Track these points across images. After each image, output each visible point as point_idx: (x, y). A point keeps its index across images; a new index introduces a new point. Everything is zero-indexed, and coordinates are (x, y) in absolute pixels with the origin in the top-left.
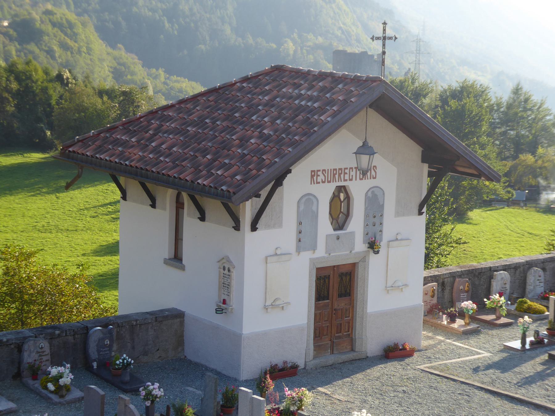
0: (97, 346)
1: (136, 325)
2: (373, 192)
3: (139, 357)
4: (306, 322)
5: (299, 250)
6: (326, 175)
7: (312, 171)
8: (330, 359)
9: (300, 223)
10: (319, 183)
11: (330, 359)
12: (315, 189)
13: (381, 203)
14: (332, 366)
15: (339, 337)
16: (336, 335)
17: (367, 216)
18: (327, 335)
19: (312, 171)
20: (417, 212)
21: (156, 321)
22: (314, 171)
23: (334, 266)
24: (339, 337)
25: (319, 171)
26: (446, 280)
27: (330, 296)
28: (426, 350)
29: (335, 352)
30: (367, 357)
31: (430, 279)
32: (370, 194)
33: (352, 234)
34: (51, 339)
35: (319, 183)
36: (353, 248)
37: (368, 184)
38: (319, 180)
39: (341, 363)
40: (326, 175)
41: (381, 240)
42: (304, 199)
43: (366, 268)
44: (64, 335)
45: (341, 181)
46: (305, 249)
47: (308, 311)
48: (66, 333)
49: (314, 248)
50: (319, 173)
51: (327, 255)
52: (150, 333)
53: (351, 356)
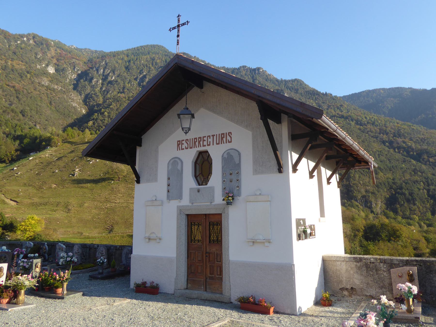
2: (228, 154)
4: (175, 255)
5: (169, 198)
7: (178, 141)
9: (169, 179)
10: (183, 149)
13: (237, 162)
19: (178, 141)
25: (184, 140)
30: (231, 303)
32: (225, 156)
35: (183, 149)
37: (224, 147)
38: (184, 147)
41: (239, 195)
49: (180, 197)
50: (183, 142)
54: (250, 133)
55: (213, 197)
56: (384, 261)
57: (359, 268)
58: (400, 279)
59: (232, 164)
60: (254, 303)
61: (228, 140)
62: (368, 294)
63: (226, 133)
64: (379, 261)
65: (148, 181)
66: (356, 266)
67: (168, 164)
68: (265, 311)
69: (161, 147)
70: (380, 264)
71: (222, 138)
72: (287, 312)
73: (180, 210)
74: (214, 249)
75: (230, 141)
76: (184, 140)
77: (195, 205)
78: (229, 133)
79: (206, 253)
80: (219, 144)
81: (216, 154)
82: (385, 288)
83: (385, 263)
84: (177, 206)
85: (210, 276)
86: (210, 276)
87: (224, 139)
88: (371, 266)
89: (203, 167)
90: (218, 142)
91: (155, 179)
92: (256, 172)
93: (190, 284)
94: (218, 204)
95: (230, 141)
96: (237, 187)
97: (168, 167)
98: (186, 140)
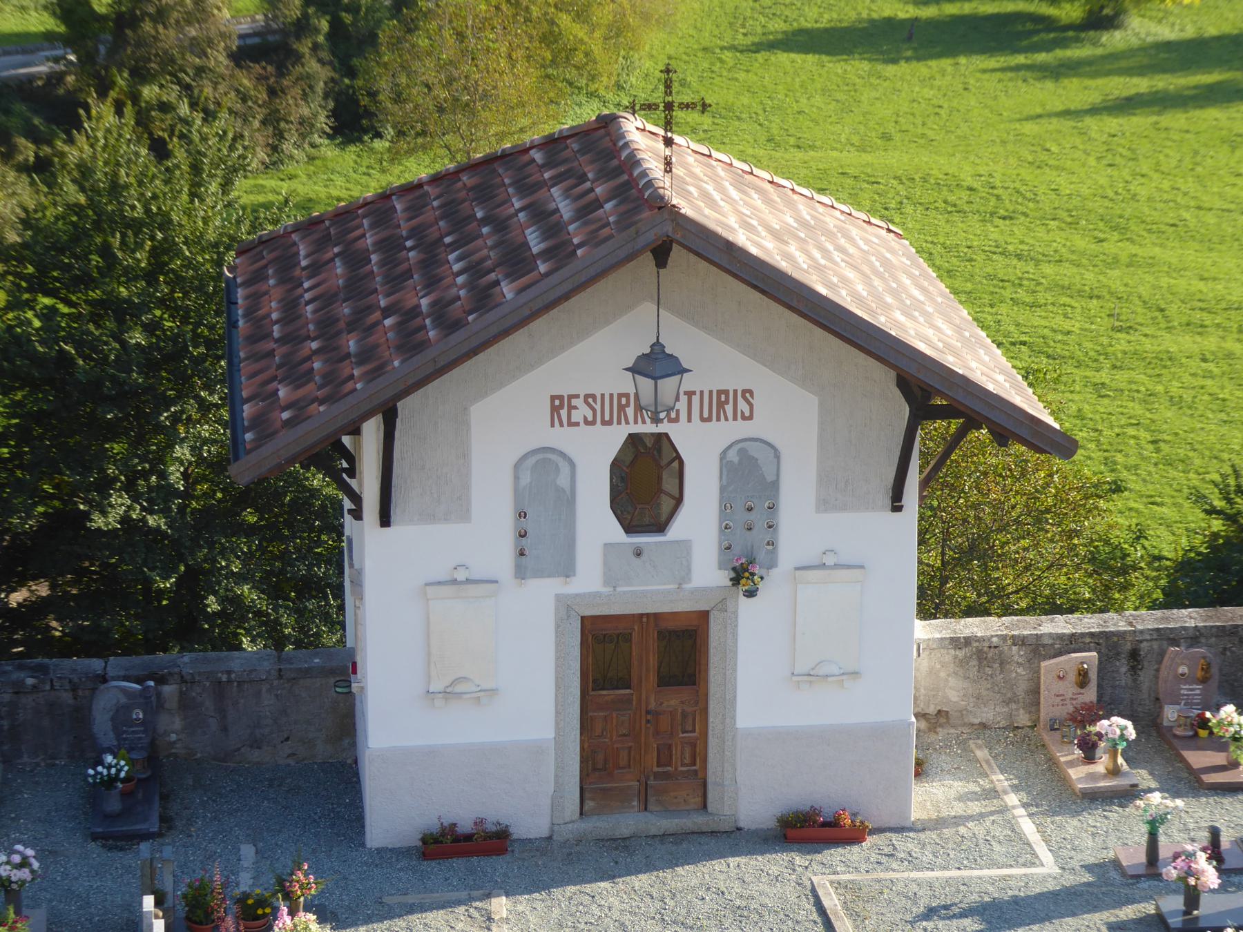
0: (112, 719)
1: (229, 681)
2: (742, 452)
3: (239, 749)
4: (550, 734)
5: (521, 573)
6: (598, 407)
7: (553, 398)
8: (628, 822)
9: (522, 515)
10: (577, 424)
11: (604, 824)
12: (561, 438)
13: (770, 478)
14: (663, 837)
15: (666, 776)
16: (656, 769)
17: (725, 507)
18: (629, 766)
19: (553, 398)
20: (888, 502)
21: (280, 677)
22: (561, 398)
23: (642, 615)
24: (666, 776)
25: (577, 396)
26: (1145, 644)
27: (635, 681)
28: (924, 830)
29: (650, 807)
30: (739, 829)
31: (1088, 640)
32: (733, 456)
33: (684, 547)
34: (16, 693)
35: (577, 424)
36: (687, 577)
37: (727, 431)
38: (577, 416)
39: (654, 836)
40: (598, 407)
41: (772, 564)
42: (531, 461)
43: (732, 625)
44: (48, 687)
45: (627, 422)
46: (540, 573)
47: (557, 712)
48: (52, 685)
49: (567, 569)
50: (574, 402)
51: (607, 590)
52: (266, 703)
53: (696, 821)
54: (814, 400)
55: (689, 570)
56: (1020, 641)
57: (962, 663)
58: (1061, 683)
59: (752, 485)
60: (834, 824)
61: (742, 413)
62: (977, 721)
63: (735, 392)
64: (1009, 642)
65: (429, 517)
66: (956, 657)
67: (517, 466)
68: (853, 836)
69: (479, 412)
70: (1010, 649)
71: (721, 405)
72: (1144, 840)
73: (565, 605)
74: (673, 702)
75: (747, 414)
76: (577, 396)
77: (625, 593)
78: (744, 392)
79: (648, 712)
80: (709, 419)
81: (700, 448)
82: (1017, 702)
83: (1023, 644)
84: (557, 596)
85: (660, 770)
86: (660, 770)
87: (729, 408)
88: (990, 655)
89: (645, 486)
90: (706, 415)
91: (457, 507)
92: (824, 505)
93: (593, 799)
94: (705, 589)
95: (747, 414)
96: (768, 544)
97: (516, 478)
98: (587, 396)
